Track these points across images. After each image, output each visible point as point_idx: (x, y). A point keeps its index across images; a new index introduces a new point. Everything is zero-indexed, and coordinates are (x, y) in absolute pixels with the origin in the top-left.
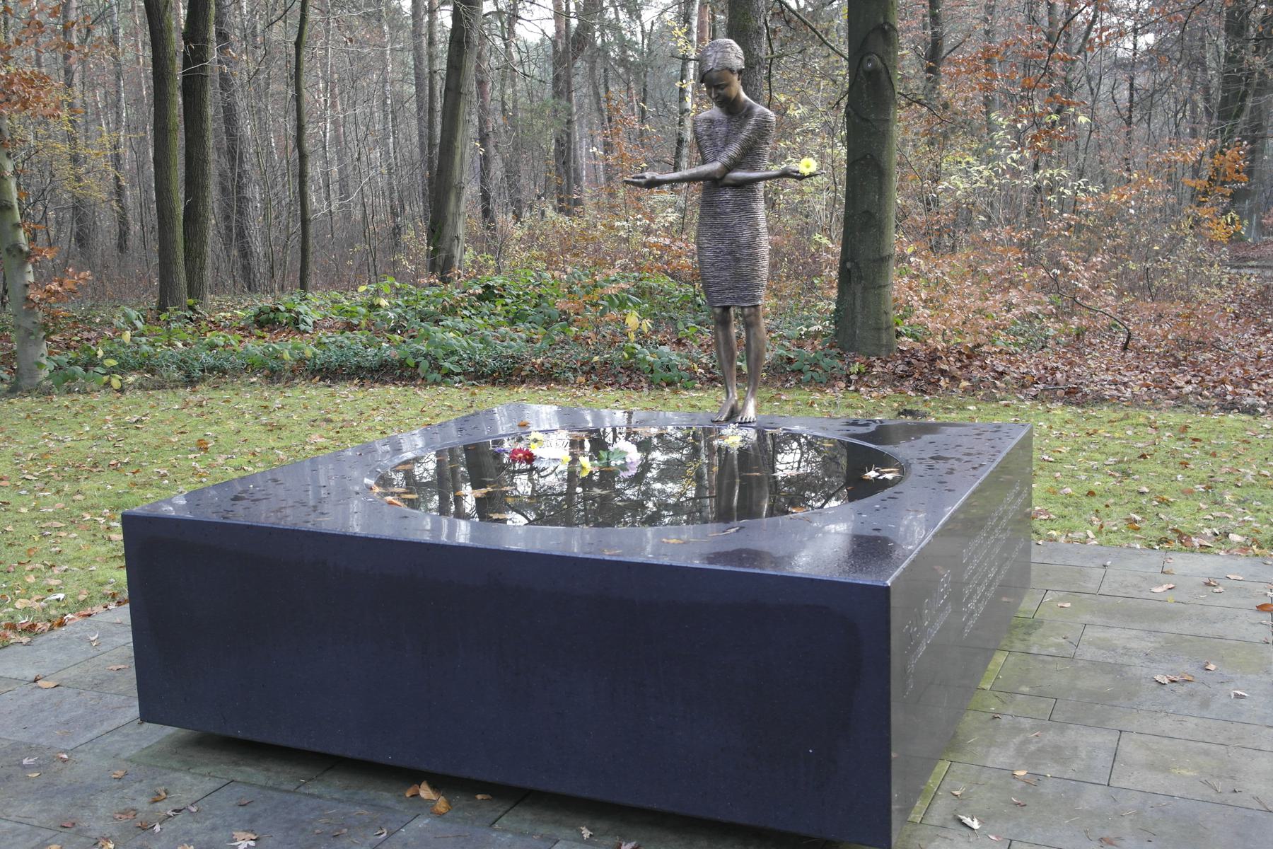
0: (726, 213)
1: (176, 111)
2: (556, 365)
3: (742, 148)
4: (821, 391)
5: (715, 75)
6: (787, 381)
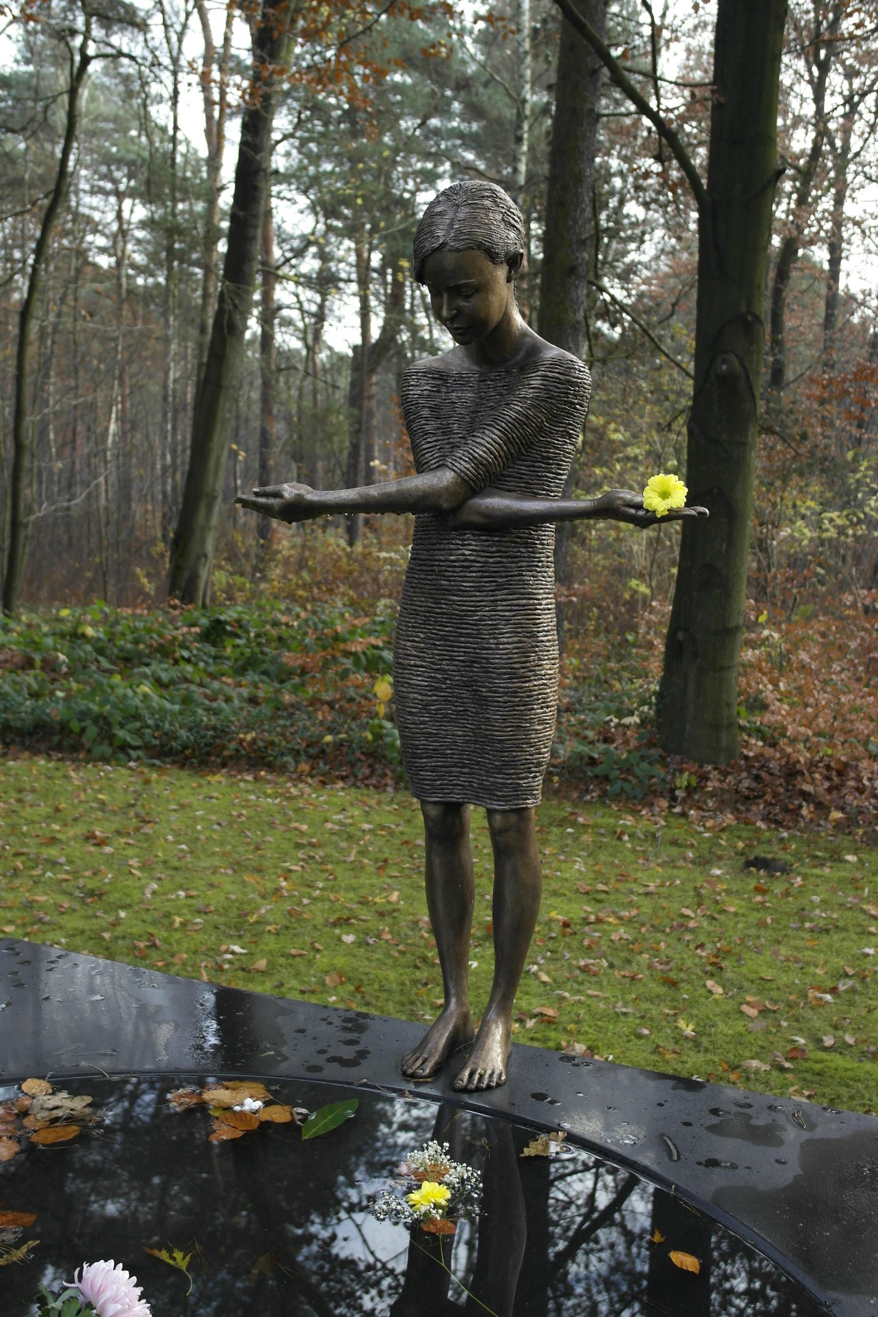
0: (460, 592)
1: (435, 481)
2: (272, 743)
3: (508, 441)
4: (635, 812)
5: (449, 260)
6: (587, 791)
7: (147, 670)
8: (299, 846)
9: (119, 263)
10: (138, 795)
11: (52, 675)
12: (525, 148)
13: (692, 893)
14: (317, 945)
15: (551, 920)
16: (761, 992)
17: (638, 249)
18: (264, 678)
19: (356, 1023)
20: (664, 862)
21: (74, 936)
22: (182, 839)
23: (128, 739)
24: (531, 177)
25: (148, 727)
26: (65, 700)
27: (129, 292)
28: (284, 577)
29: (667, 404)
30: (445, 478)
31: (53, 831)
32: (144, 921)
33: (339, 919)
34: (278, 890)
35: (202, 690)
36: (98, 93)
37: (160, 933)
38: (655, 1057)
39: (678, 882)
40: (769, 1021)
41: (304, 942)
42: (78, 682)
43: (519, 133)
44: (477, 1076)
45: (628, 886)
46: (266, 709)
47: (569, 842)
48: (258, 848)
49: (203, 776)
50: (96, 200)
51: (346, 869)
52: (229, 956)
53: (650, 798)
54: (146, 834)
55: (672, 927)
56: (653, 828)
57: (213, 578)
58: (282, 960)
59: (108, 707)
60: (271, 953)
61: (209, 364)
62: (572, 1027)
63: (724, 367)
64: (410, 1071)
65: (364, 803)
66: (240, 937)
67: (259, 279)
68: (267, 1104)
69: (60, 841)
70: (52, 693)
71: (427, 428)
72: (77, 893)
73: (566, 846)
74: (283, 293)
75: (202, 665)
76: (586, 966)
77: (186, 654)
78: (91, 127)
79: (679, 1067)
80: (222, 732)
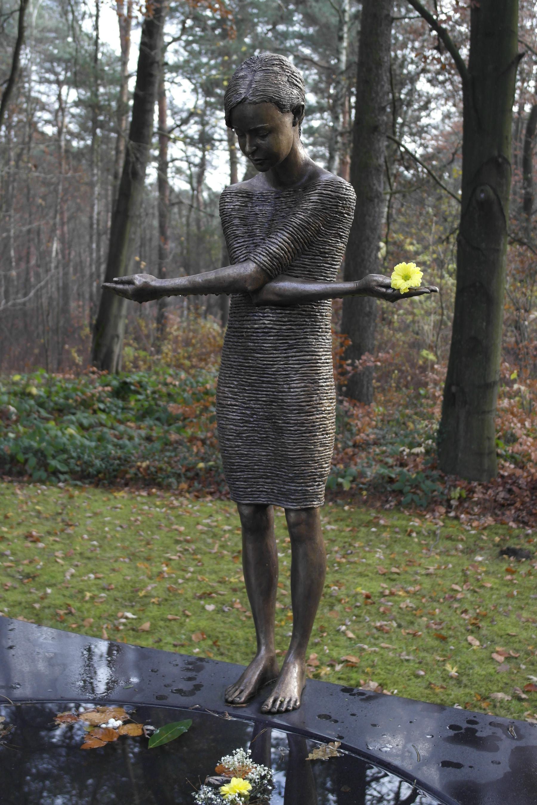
0: (262, 351)
1: (242, 270)
2: (161, 469)
3: (294, 241)
4: (421, 516)
5: (249, 110)
6: (387, 501)
7: (73, 418)
8: (177, 542)
9: (60, 132)
10: (64, 506)
11: (6, 422)
12: (345, 44)
13: (460, 574)
14: (187, 612)
15: (357, 594)
16: (507, 644)
17: (428, 115)
18: (158, 423)
19: (196, 665)
20: (441, 552)
21: (13, 606)
22: (94, 537)
23: (59, 466)
24: (349, 65)
25: (72, 458)
26: (15, 439)
27: (67, 151)
28: (175, 350)
29: (447, 224)
30: (250, 268)
31: (3, 532)
32: (64, 596)
33: (204, 593)
34: (160, 573)
35: (112, 431)
36: (44, 12)
37: (75, 604)
38: (428, 691)
39: (450, 566)
40: (512, 665)
41: (178, 611)
42: (25, 427)
43: (340, 34)
44: (278, 703)
45: (414, 569)
46: (158, 445)
47: (373, 537)
48: (148, 544)
49: (111, 493)
50: (43, 88)
51: (211, 558)
52: (123, 620)
53: (432, 506)
54: (68, 534)
55: (444, 598)
56: (434, 528)
57: (124, 353)
58: (162, 623)
59: (44, 444)
60: (153, 618)
61: (119, 201)
62: (368, 670)
63: (482, 195)
64: (230, 699)
65: (226, 511)
66: (132, 606)
67: (155, 140)
68: (125, 723)
69: (7, 539)
70: (6, 435)
71: (238, 232)
72: (18, 576)
73: (371, 541)
74: (175, 150)
75: (113, 413)
76: (381, 626)
77: (102, 406)
78: (39, 36)
79: (445, 698)
80: (125, 461)
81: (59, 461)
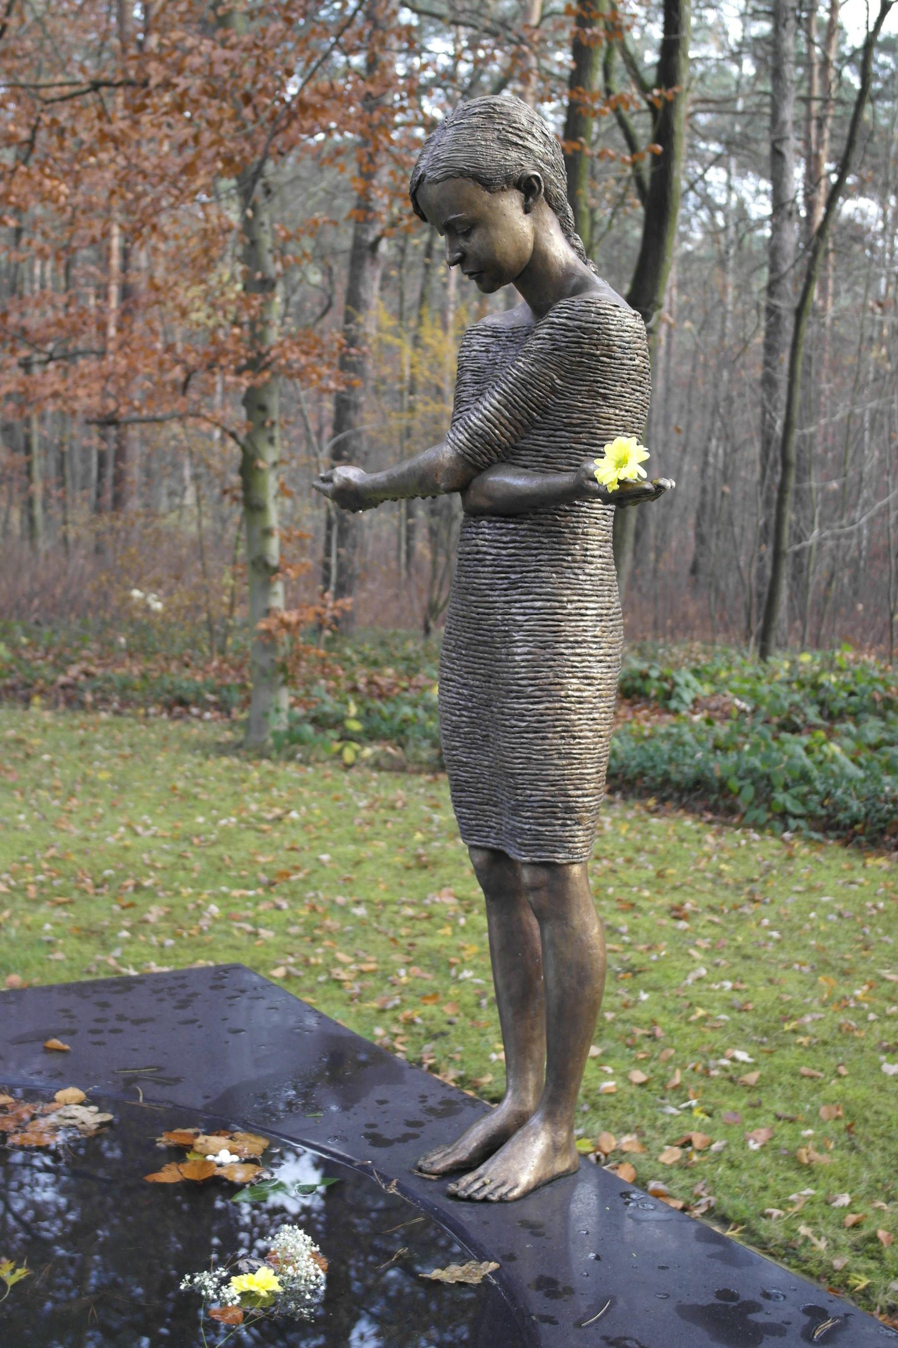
81: (795, 797)
